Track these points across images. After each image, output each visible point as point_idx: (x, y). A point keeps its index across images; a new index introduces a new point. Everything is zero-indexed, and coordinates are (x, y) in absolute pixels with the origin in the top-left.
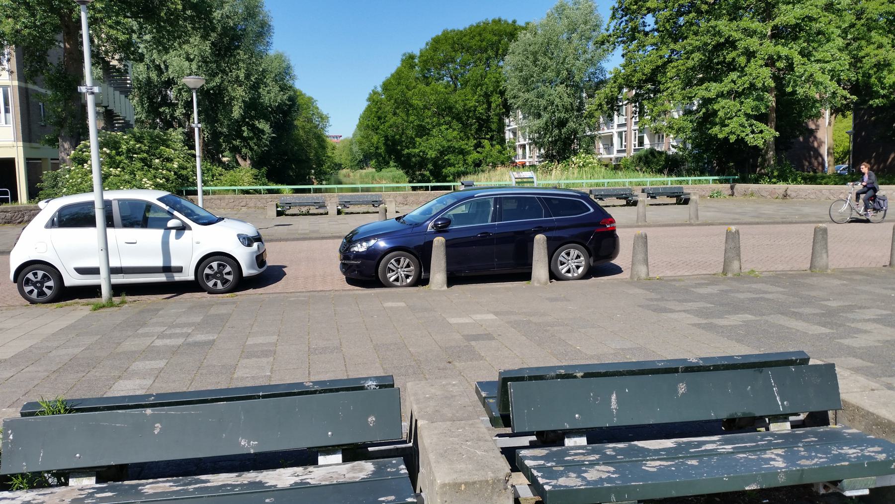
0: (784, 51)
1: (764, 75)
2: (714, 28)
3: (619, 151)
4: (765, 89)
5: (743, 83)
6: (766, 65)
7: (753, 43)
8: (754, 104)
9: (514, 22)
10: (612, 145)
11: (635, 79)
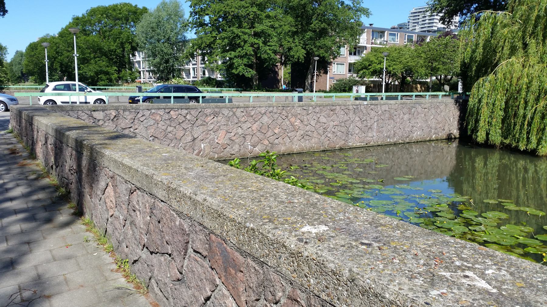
0: (257, 41)
1: (249, 50)
2: (232, 30)
3: (193, 77)
4: (251, 55)
5: (243, 53)
6: (251, 46)
7: (246, 37)
8: (247, 60)
9: (136, 6)
10: (190, 74)
11: (203, 46)
